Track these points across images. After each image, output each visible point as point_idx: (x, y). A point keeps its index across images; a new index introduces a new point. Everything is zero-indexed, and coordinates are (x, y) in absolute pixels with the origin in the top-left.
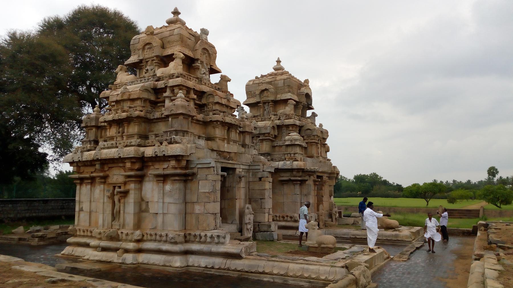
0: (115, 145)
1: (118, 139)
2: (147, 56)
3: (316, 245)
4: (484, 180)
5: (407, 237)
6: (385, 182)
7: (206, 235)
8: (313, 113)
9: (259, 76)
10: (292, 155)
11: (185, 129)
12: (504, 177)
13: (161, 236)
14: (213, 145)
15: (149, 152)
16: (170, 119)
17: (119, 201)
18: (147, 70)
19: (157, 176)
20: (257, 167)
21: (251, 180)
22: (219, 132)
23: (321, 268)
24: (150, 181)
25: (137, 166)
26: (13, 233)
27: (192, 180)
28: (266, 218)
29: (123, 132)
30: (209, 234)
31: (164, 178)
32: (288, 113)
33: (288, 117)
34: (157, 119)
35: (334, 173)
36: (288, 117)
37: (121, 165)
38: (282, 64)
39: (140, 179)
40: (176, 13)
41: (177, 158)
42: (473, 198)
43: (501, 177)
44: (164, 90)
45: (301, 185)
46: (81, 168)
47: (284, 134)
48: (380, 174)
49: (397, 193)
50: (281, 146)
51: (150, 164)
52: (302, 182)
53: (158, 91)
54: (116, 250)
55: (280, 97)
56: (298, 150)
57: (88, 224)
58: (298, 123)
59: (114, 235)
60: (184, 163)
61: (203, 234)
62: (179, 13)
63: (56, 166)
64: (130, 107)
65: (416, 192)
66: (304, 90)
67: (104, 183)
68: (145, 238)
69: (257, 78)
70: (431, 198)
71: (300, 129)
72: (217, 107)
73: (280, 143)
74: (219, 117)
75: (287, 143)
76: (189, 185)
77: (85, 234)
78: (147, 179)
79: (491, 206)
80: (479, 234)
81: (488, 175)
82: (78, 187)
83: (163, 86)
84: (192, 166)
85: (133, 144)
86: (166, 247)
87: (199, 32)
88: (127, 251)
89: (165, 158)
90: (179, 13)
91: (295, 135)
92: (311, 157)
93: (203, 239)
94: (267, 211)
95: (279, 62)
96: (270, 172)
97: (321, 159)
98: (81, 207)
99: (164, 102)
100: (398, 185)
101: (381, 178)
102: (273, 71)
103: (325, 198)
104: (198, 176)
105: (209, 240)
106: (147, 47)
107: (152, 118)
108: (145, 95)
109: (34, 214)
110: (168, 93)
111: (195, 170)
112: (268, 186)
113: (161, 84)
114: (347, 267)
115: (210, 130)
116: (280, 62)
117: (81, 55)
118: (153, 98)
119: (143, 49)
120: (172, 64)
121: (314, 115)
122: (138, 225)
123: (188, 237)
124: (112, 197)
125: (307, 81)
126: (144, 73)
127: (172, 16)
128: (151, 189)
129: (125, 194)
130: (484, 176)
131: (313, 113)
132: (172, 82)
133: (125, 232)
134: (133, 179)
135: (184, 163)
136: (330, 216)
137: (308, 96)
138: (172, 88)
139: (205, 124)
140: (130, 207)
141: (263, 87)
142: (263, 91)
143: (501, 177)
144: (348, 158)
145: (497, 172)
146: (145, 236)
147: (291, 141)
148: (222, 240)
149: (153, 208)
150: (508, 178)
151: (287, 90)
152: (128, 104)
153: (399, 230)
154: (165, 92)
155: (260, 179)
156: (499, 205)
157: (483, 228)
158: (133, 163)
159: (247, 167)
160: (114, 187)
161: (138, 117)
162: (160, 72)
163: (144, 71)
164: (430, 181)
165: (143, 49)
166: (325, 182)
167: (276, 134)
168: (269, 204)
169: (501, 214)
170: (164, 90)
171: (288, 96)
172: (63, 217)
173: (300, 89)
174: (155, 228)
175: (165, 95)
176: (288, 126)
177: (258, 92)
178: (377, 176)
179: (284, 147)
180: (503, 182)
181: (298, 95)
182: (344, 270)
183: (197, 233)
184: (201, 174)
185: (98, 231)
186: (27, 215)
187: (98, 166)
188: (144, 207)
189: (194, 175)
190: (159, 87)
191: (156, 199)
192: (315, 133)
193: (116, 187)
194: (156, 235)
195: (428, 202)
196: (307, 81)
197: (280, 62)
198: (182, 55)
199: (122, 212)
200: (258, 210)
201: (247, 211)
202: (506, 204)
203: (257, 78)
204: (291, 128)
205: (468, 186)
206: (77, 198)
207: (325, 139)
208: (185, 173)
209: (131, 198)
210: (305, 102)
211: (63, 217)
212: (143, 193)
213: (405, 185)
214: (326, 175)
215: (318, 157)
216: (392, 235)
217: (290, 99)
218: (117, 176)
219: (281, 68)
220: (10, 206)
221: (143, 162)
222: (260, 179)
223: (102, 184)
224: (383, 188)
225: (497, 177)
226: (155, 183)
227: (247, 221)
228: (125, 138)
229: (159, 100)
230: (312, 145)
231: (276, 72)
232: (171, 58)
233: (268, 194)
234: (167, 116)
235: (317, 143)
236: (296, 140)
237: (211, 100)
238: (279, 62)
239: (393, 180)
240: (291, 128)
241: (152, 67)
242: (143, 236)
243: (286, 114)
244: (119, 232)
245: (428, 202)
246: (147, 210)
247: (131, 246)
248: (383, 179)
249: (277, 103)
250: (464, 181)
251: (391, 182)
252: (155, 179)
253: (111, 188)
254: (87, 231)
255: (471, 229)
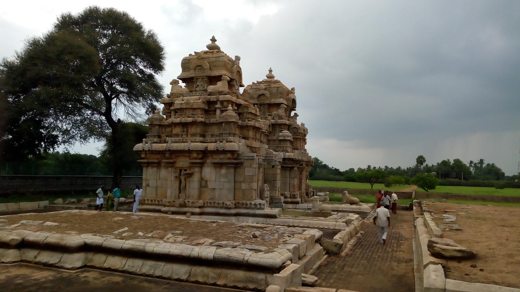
0: (182, 141)
1: (184, 136)
2: (197, 75)
3: (319, 211)
4: (412, 167)
5: (366, 209)
6: (325, 166)
7: (251, 203)
8: (295, 114)
9: (256, 82)
10: (285, 148)
11: (233, 132)
12: (430, 165)
13: (218, 204)
14: (249, 142)
15: (211, 146)
16: (224, 125)
17: (185, 179)
18: (198, 85)
19: (214, 164)
20: (271, 158)
21: (266, 167)
22: (251, 134)
23: (331, 223)
24: (208, 167)
25: (200, 156)
26: (55, 204)
27: (240, 167)
28: (277, 194)
29: (188, 132)
30: (253, 203)
31: (219, 165)
32: (280, 114)
33: (281, 118)
34: (213, 123)
35: (310, 162)
36: (221, 93)
37: (187, 155)
38: (273, 73)
39: (201, 165)
40: (213, 40)
41: (233, 152)
42: (407, 182)
43: (427, 165)
44: (215, 103)
45: (290, 170)
46: (148, 155)
47: (277, 131)
48: (320, 159)
49: (332, 176)
50: (274, 140)
51: (209, 155)
52: (292, 168)
53: (210, 103)
54: (184, 213)
55: (273, 101)
56: (288, 144)
57: (155, 196)
58: (288, 122)
59: (183, 203)
60: (236, 156)
61: (248, 203)
62: (216, 41)
63: (67, 147)
64: (193, 114)
65: (350, 176)
66: (291, 96)
67: (172, 167)
68: (206, 205)
69: (253, 83)
70: (374, 183)
71: (289, 127)
72: (250, 116)
73: (275, 138)
74: (252, 123)
75: (280, 138)
76: (238, 170)
77: (154, 202)
78: (206, 165)
79: (421, 190)
80: (414, 208)
81: (416, 163)
82: (144, 169)
83: (215, 100)
84: (241, 158)
85: (197, 140)
86: (222, 211)
87: (234, 59)
88: (193, 214)
89: (224, 152)
90: (216, 41)
91: (286, 132)
92: (297, 149)
93: (249, 206)
94: (277, 189)
95: (271, 71)
96: (279, 162)
97: (303, 151)
98: (147, 183)
99: (215, 111)
100: (336, 169)
101: (321, 162)
102: (266, 78)
103: (303, 181)
104: (245, 164)
105: (253, 206)
106: (198, 68)
107: (208, 122)
108: (203, 106)
109: (49, 189)
110: (218, 105)
111: (243, 161)
112: (279, 171)
113: (213, 98)
114: (346, 223)
115: (246, 132)
116: (272, 71)
117: (95, 55)
118: (207, 108)
119: (195, 69)
120: (219, 84)
121: (296, 115)
122: (200, 197)
123: (237, 205)
124: (178, 178)
125: (293, 89)
126: (195, 87)
127: (210, 42)
128: (208, 172)
129: (191, 175)
130: (413, 164)
131: (295, 114)
132: (222, 98)
133: (191, 201)
134: (198, 165)
135: (236, 156)
136: (307, 194)
137: (294, 101)
138: (222, 102)
139: (242, 127)
140: (194, 185)
141: (261, 92)
142: (260, 96)
143: (427, 165)
144: (315, 148)
145: (425, 161)
146: (206, 204)
147: (284, 137)
148: (262, 206)
149: (211, 185)
150: (433, 165)
151: (279, 96)
152: (191, 112)
153: (360, 205)
154: (216, 104)
155: (273, 167)
156: (426, 189)
157: (417, 205)
158: (198, 154)
159: (264, 158)
160: (181, 171)
161: (201, 122)
162: (211, 88)
163: (195, 85)
164: (364, 167)
165: (195, 69)
166: (304, 168)
167: (271, 130)
168: (278, 184)
169: (428, 196)
170: (215, 103)
171: (281, 100)
172: (73, 192)
173: (288, 95)
174: (213, 199)
175: (217, 106)
176: (280, 125)
177: (256, 96)
178: (319, 160)
179: (277, 142)
180: (429, 170)
181: (287, 100)
182: (344, 224)
183: (244, 202)
184: (246, 164)
185: (168, 200)
186: (44, 189)
187: (167, 155)
188: (203, 184)
189: (242, 164)
190: (211, 100)
191: (213, 179)
192: (299, 131)
193: (183, 171)
194: (214, 203)
195: (372, 186)
196: (293, 89)
197: (272, 71)
198: (229, 79)
199: (187, 187)
200: (273, 188)
201: (266, 189)
202: (431, 189)
203: (253, 83)
204: (282, 127)
205: (398, 172)
206: (144, 177)
207: (305, 135)
208: (234, 162)
209: (196, 178)
210: (292, 104)
211: (73, 192)
212: (203, 174)
213: (342, 169)
214: (305, 163)
215: (301, 149)
216: (357, 208)
217: (283, 104)
218: (183, 162)
219: (273, 77)
220: (30, 181)
221: (205, 153)
222: (273, 167)
223: (170, 167)
224: (324, 171)
225: (424, 164)
226: (213, 168)
227: (266, 196)
228: (189, 136)
229: (210, 109)
230: (297, 140)
231: (269, 80)
232: (219, 78)
233: (279, 177)
234: (222, 123)
235: (300, 139)
236: (288, 136)
237: (246, 110)
238: (271, 71)
239: (332, 164)
240: (282, 127)
241: (202, 83)
242: (204, 204)
243: (279, 115)
244: (186, 201)
245: (372, 186)
246: (206, 186)
247: (197, 210)
248: (323, 163)
249: (271, 105)
250: (395, 167)
251: (330, 166)
252: (213, 166)
253: (178, 171)
254: (155, 200)
255: (408, 206)
